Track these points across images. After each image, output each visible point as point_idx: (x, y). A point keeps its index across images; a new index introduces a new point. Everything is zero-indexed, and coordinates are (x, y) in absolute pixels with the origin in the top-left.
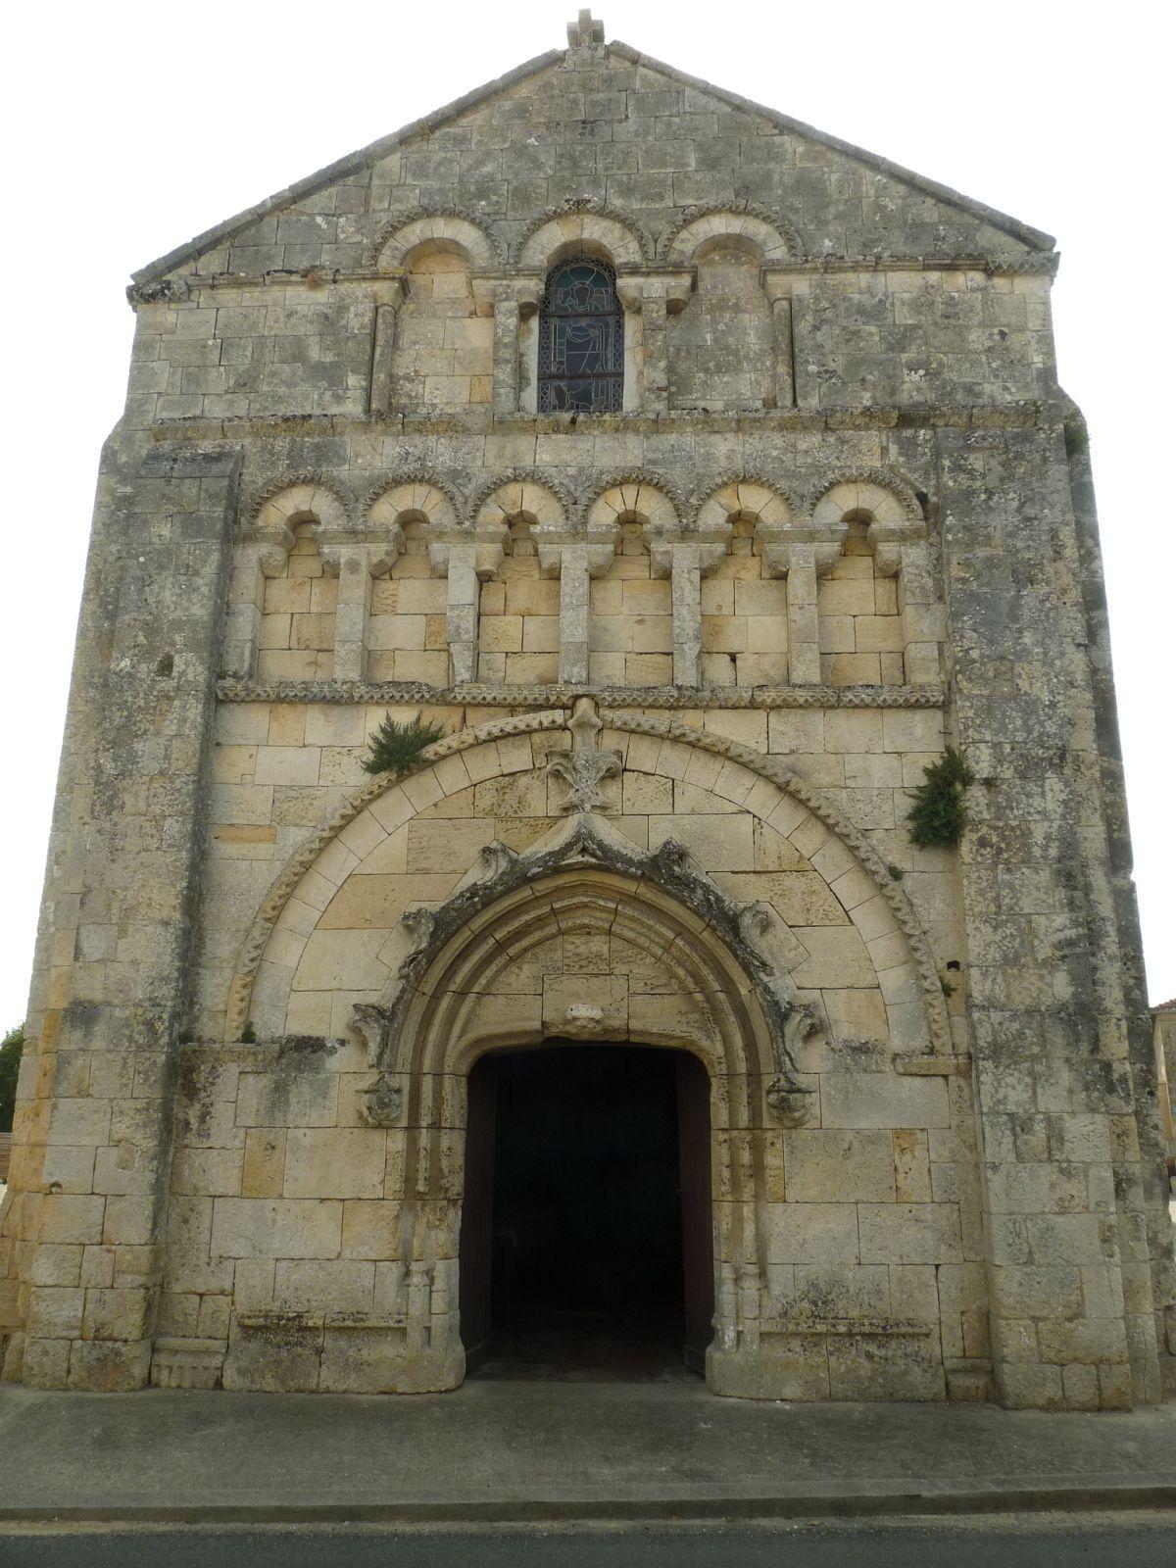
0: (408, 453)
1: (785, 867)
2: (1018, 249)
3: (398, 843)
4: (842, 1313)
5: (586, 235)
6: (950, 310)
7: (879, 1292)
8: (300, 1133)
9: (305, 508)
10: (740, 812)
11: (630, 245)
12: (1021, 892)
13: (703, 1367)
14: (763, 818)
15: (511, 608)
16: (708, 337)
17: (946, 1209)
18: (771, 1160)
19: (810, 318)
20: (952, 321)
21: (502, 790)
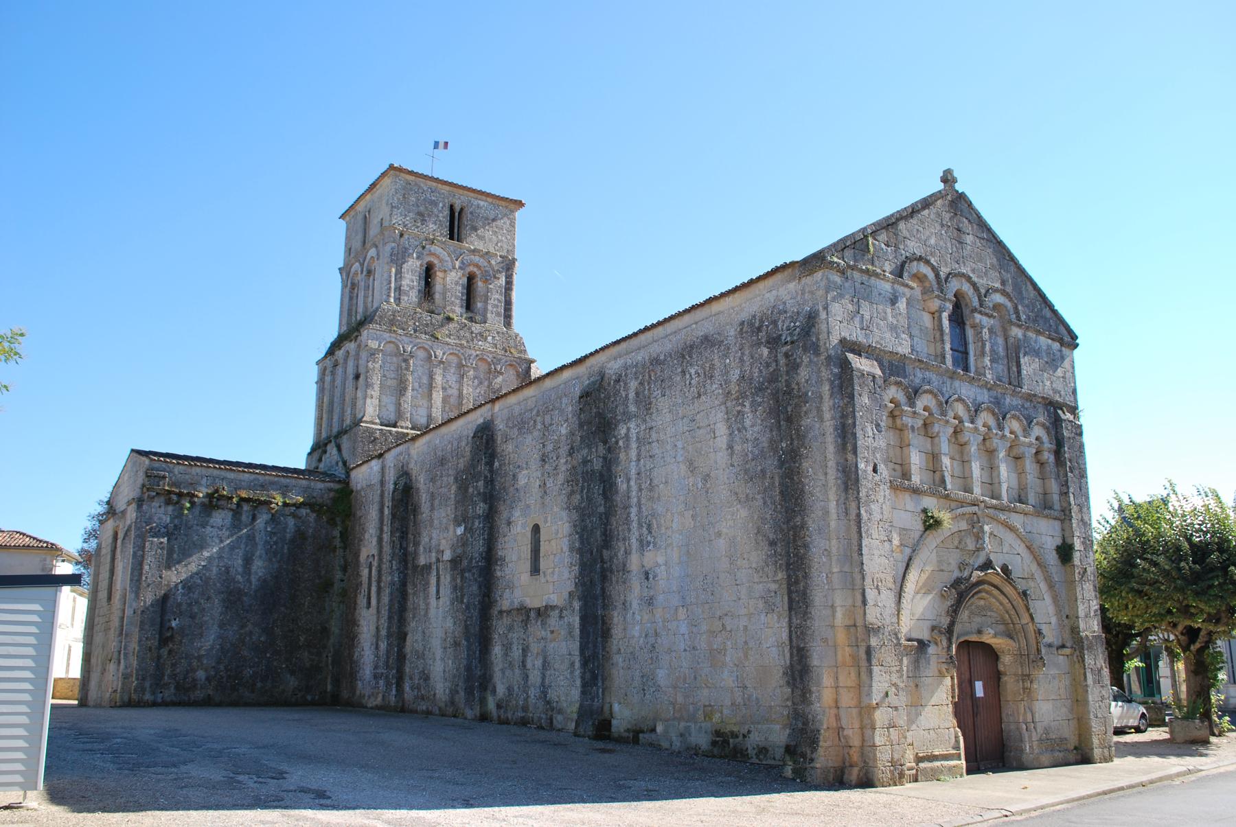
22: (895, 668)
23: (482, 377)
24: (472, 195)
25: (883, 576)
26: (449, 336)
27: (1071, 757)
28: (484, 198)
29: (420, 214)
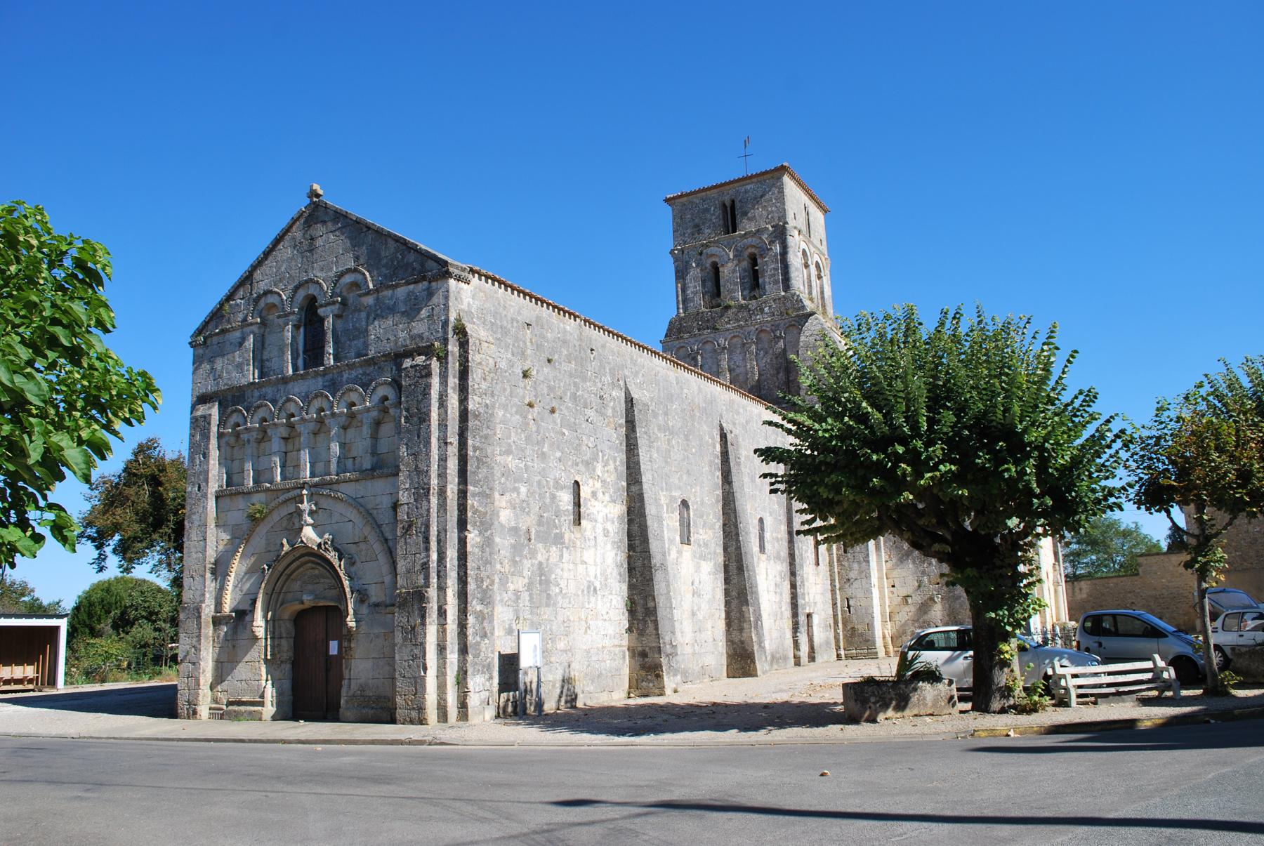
3: (263, 541)
20: (416, 307)
23: (766, 346)
24: (738, 184)
25: (197, 567)
26: (728, 323)
29: (697, 226)
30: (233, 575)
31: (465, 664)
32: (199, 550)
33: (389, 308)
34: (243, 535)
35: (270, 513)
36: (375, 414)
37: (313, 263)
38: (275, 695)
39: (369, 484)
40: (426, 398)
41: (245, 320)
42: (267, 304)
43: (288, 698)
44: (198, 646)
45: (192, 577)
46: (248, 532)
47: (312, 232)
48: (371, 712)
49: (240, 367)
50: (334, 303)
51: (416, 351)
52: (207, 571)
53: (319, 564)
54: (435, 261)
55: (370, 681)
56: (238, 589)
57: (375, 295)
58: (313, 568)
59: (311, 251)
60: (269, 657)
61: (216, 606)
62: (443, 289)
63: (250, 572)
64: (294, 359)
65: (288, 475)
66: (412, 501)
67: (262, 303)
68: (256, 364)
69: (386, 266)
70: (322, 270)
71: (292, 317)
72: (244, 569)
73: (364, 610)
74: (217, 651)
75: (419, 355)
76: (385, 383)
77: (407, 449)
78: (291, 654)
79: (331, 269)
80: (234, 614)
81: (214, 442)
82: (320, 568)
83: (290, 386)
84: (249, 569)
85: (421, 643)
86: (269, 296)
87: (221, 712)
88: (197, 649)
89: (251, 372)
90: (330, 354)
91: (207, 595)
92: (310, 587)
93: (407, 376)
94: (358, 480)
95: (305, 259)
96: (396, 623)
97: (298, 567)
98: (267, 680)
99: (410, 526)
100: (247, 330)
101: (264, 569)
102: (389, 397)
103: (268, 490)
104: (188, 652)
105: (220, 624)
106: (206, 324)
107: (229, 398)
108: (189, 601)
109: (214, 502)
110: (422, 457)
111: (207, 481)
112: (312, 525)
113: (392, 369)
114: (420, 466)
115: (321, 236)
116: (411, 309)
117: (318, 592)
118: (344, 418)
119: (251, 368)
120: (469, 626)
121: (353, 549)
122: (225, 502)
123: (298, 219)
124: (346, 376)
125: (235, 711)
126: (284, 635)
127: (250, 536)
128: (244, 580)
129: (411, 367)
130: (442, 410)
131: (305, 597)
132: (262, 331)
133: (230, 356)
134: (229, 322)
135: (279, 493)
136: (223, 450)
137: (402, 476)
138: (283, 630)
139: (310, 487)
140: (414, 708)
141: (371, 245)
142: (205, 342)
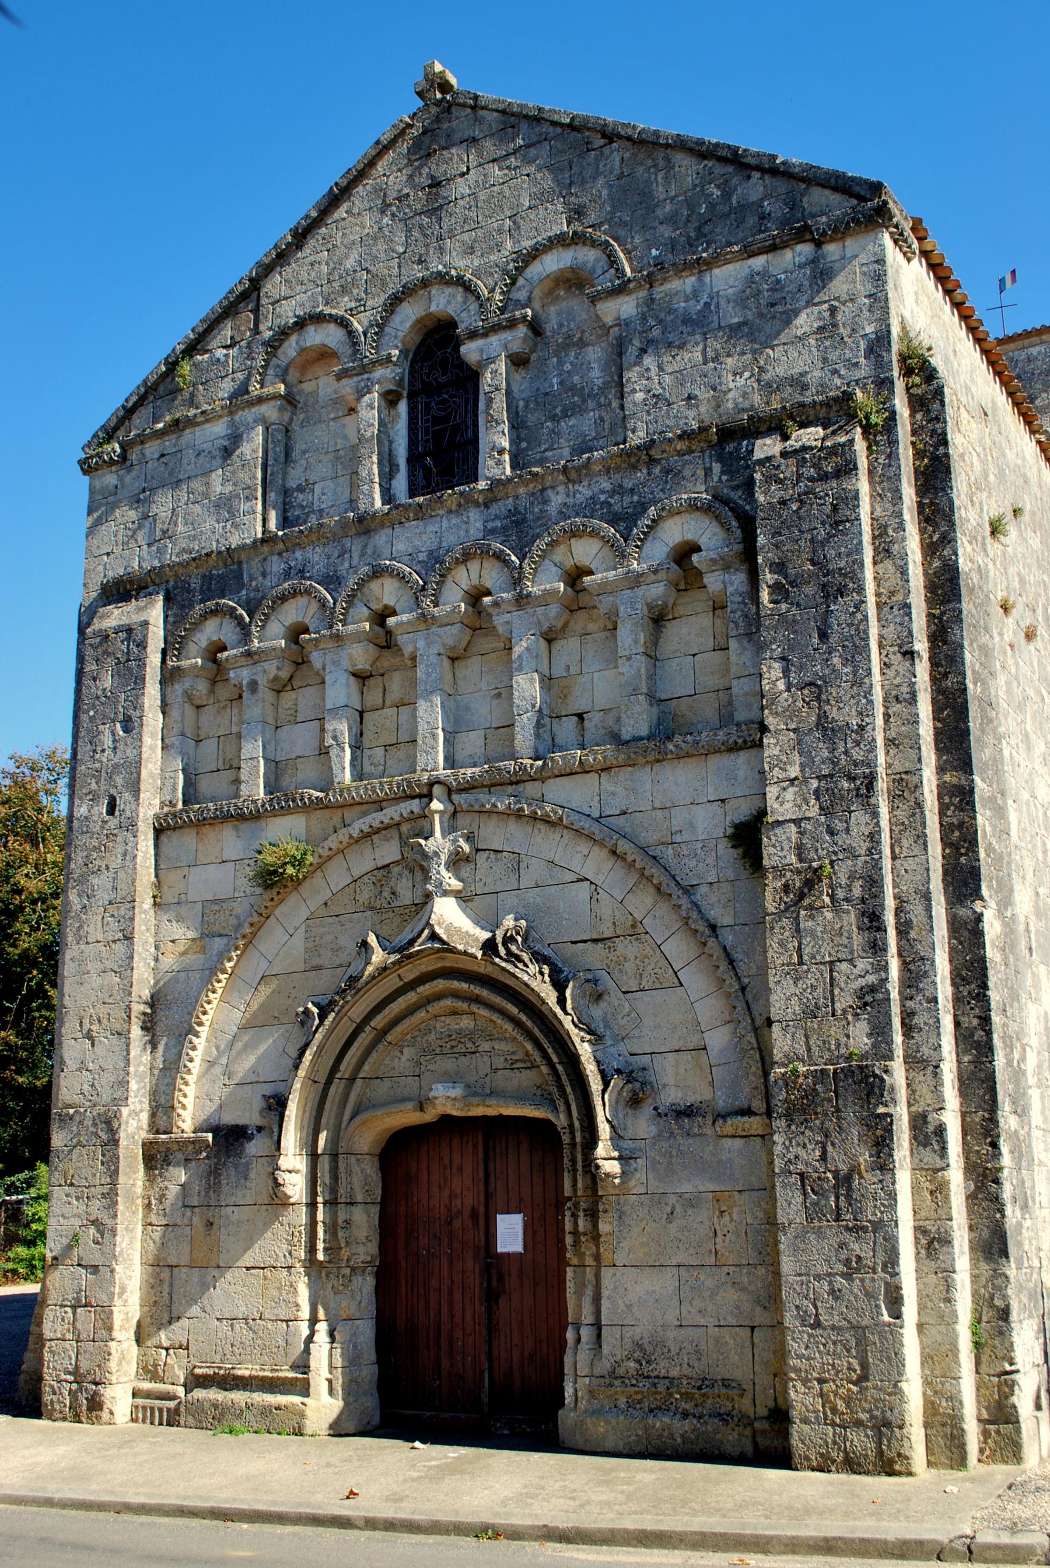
0: (290, 568)
1: (619, 932)
2: (838, 205)
3: (299, 942)
4: (663, 1373)
5: (433, 308)
6: (777, 295)
7: (698, 1352)
8: (229, 1209)
9: (215, 638)
10: (579, 880)
11: (472, 308)
12: (823, 939)
13: (1020, 1452)
14: (599, 883)
15: (388, 702)
16: (555, 381)
17: (762, 1271)
18: (604, 1227)
19: (636, 342)
20: (779, 308)
21: (379, 885)
22: (99, 1190)
24: (1012, 346)
25: (102, 1011)
27: (731, 1438)
28: (1034, 339)
30: (204, 1031)
31: (1001, 1289)
32: (109, 964)
33: (687, 320)
34: (240, 925)
35: (320, 866)
36: (656, 591)
37: (440, 238)
38: (338, 1361)
39: (645, 777)
40: (844, 533)
41: (243, 390)
42: (302, 350)
43: (369, 1372)
44: (107, 1220)
45: (89, 1036)
46: (256, 918)
47: (436, 167)
48: (681, 1427)
49: (226, 507)
50: (512, 324)
51: (791, 417)
52: (134, 1019)
53: (477, 1000)
54: (835, 189)
55: (671, 1334)
56: (218, 1070)
57: (643, 294)
58: (455, 1013)
59: (434, 211)
60: (320, 1256)
61: (153, 1115)
62: (863, 258)
63: (253, 1025)
64: (388, 475)
65: (367, 768)
66: (814, 811)
67: (290, 348)
68: (272, 496)
69: (671, 220)
70: (470, 250)
71: (379, 373)
72: (237, 1016)
73: (643, 1126)
74: (157, 1236)
75: (803, 425)
76: (694, 507)
77: (786, 672)
78: (373, 1248)
79: (499, 247)
80: (210, 1136)
81: (152, 692)
82: (484, 1012)
83: (380, 539)
84: (254, 1015)
85: (878, 1226)
86: (311, 329)
87: (172, 1404)
88: (104, 1230)
89: (259, 517)
90: (501, 452)
91: (133, 1085)
92: (448, 1064)
93: (768, 479)
94: (606, 769)
95: (416, 234)
96: (778, 1164)
97: (411, 1011)
98: (313, 1321)
99: (810, 884)
100: (247, 415)
101: (307, 1012)
102: (703, 542)
103: (318, 805)
104: (75, 1238)
105: (167, 1162)
106: (129, 412)
107: (195, 583)
108: (77, 1099)
109: (151, 842)
110: (842, 690)
111: (135, 789)
112: (458, 895)
113: (708, 471)
114: (833, 713)
115: (463, 175)
116: (761, 315)
117: (471, 1078)
118: (554, 610)
119: (259, 507)
120: (1006, 1172)
121: (594, 956)
122: (185, 842)
123: (392, 143)
124: (556, 500)
125: (215, 1405)
126: (359, 1198)
127: (257, 928)
128: (239, 1045)
129: (784, 454)
130: (888, 564)
131: (439, 1091)
132: (286, 417)
133: (197, 485)
134: (192, 402)
135: (348, 814)
136: (175, 713)
137: (771, 746)
138: (357, 1181)
139: (450, 791)
140: (859, 1423)
141: (620, 177)
142: (124, 457)
